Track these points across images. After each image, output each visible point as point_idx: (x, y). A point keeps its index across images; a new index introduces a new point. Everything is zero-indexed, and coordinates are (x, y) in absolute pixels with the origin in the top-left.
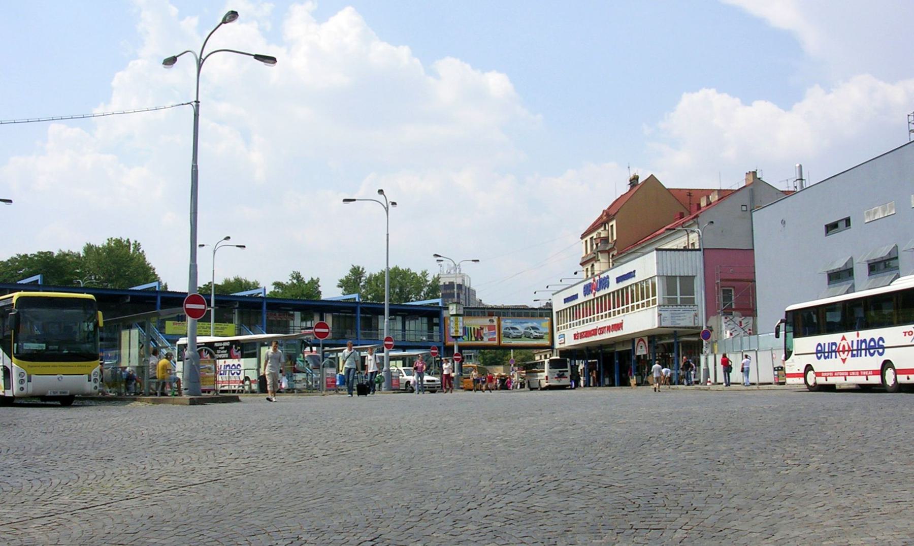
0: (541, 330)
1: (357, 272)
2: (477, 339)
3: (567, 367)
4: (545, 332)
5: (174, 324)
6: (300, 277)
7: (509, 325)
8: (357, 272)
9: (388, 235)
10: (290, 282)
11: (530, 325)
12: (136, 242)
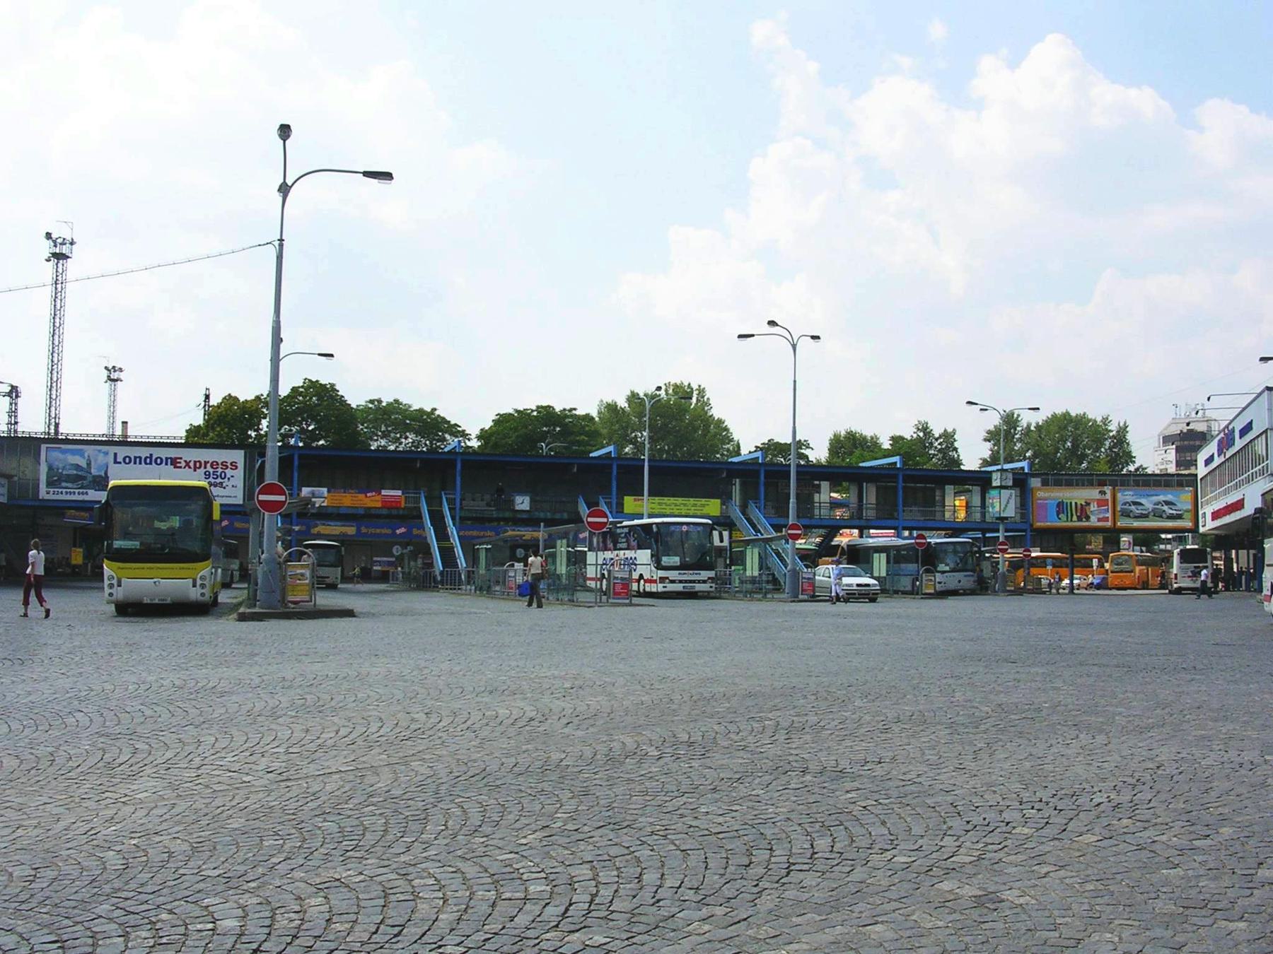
0: (1179, 506)
1: (1010, 420)
2: (1080, 519)
3: (1206, 562)
4: (1184, 508)
5: (635, 500)
6: (927, 428)
7: (1129, 499)
8: (1010, 420)
9: (795, 381)
10: (915, 436)
11: (1162, 498)
12: (700, 386)
